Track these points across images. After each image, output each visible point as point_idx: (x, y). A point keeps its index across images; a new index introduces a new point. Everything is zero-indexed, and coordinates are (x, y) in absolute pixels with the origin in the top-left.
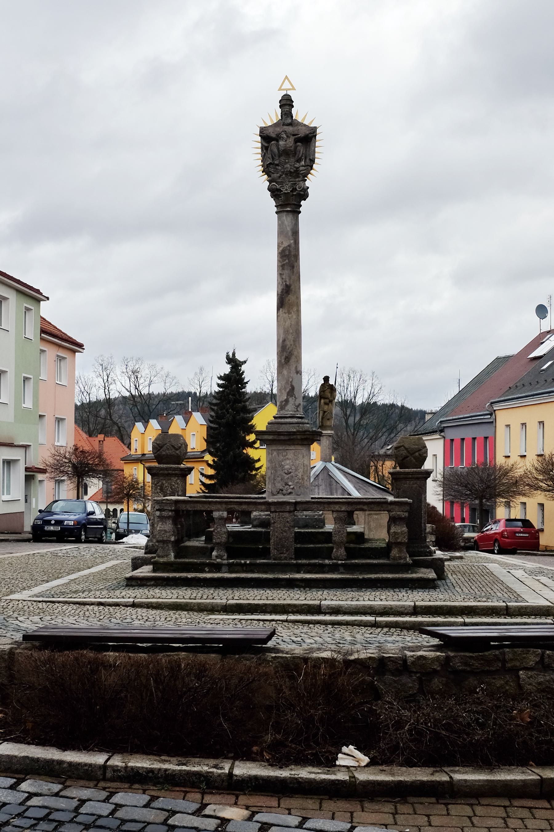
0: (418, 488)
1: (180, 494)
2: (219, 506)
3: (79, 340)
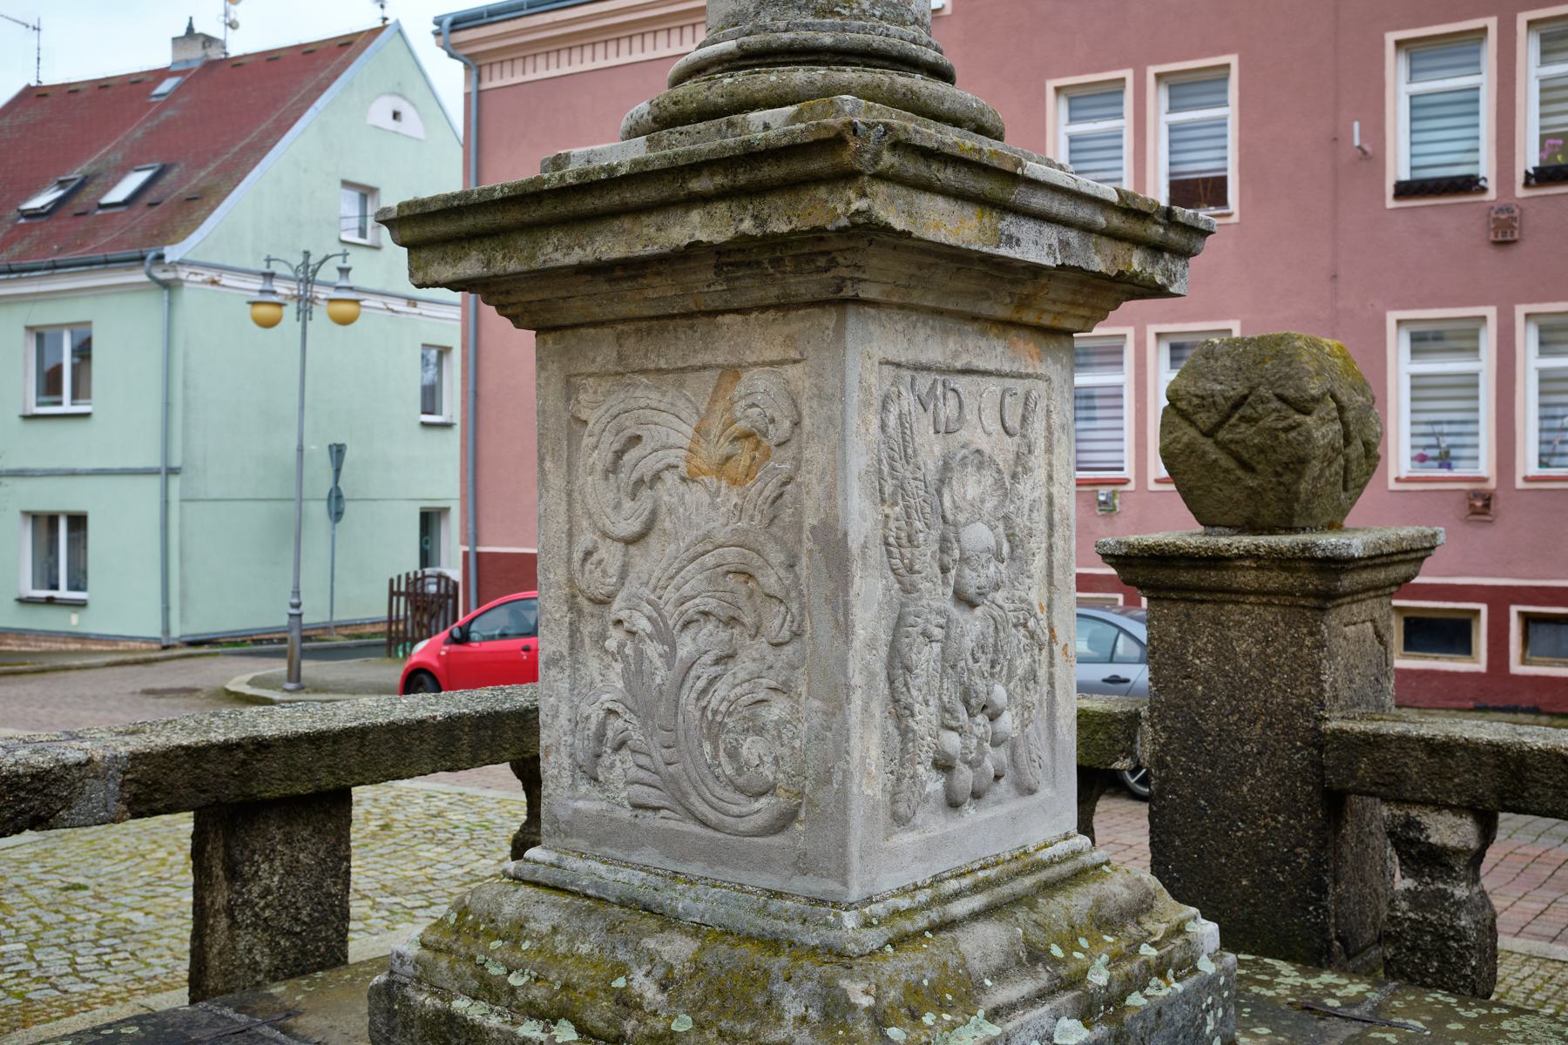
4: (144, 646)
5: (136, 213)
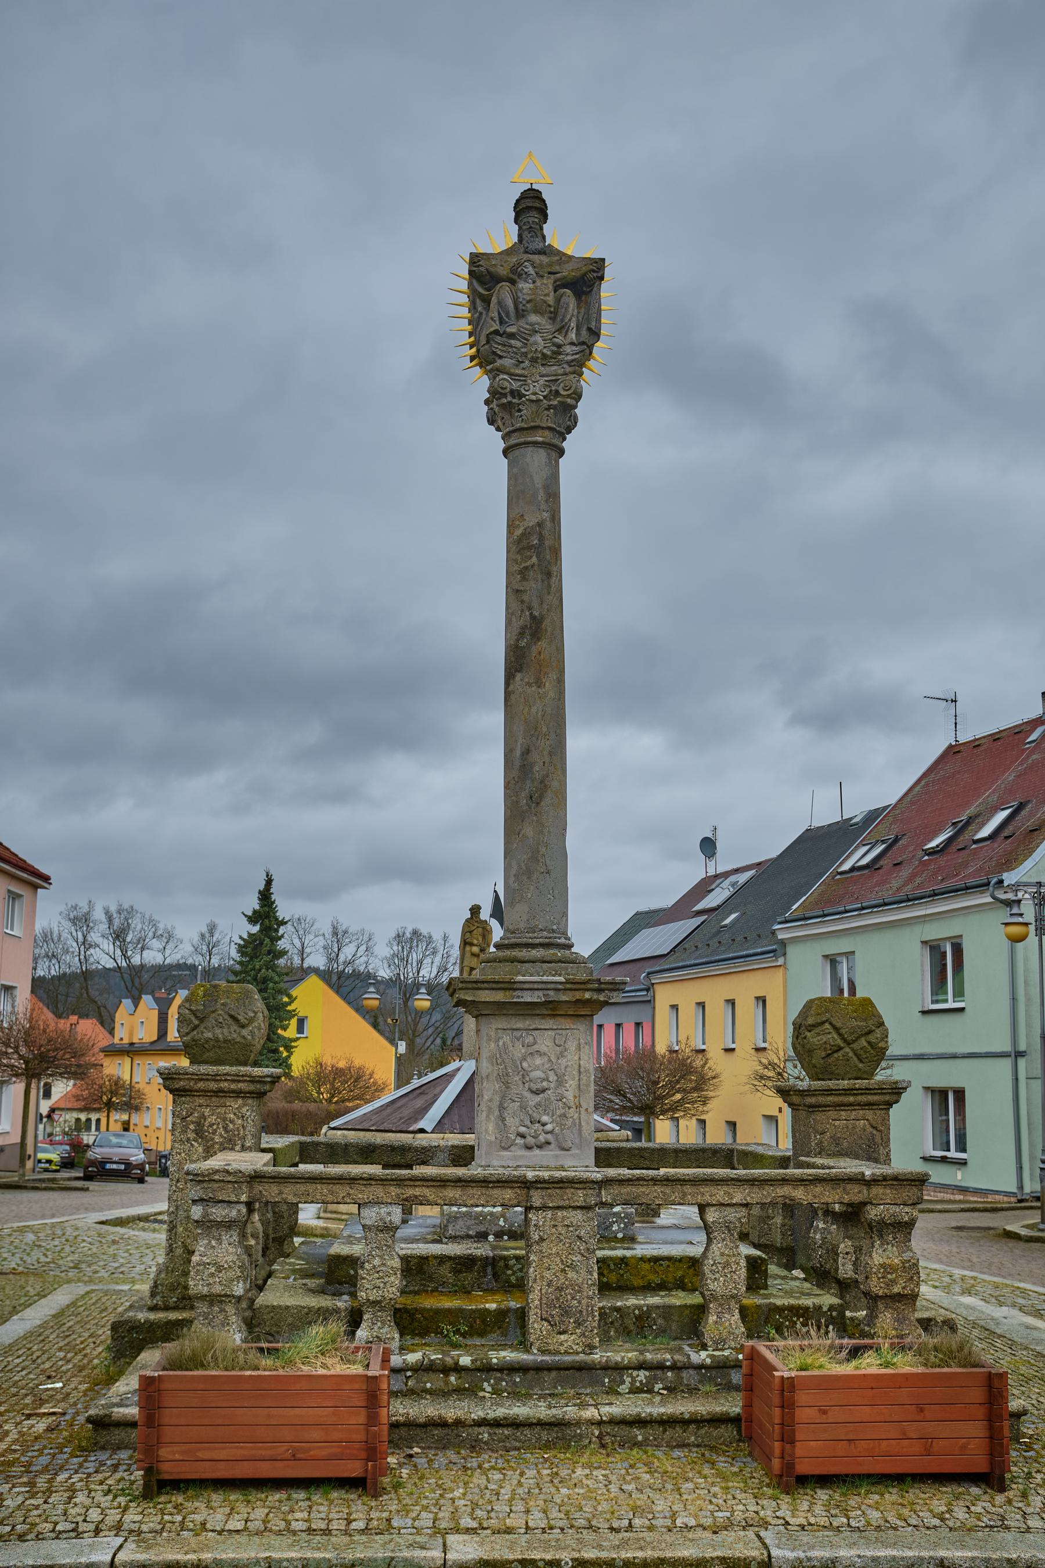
2: (379, 1191)
4: (1005, 1199)
5: (996, 845)
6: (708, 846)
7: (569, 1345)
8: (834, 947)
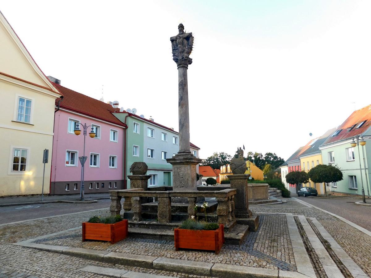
0: (241, 183)
1: (140, 187)
2: (136, 194)
3: (199, 147)
6: (311, 134)
7: (165, 222)
8: (330, 150)
